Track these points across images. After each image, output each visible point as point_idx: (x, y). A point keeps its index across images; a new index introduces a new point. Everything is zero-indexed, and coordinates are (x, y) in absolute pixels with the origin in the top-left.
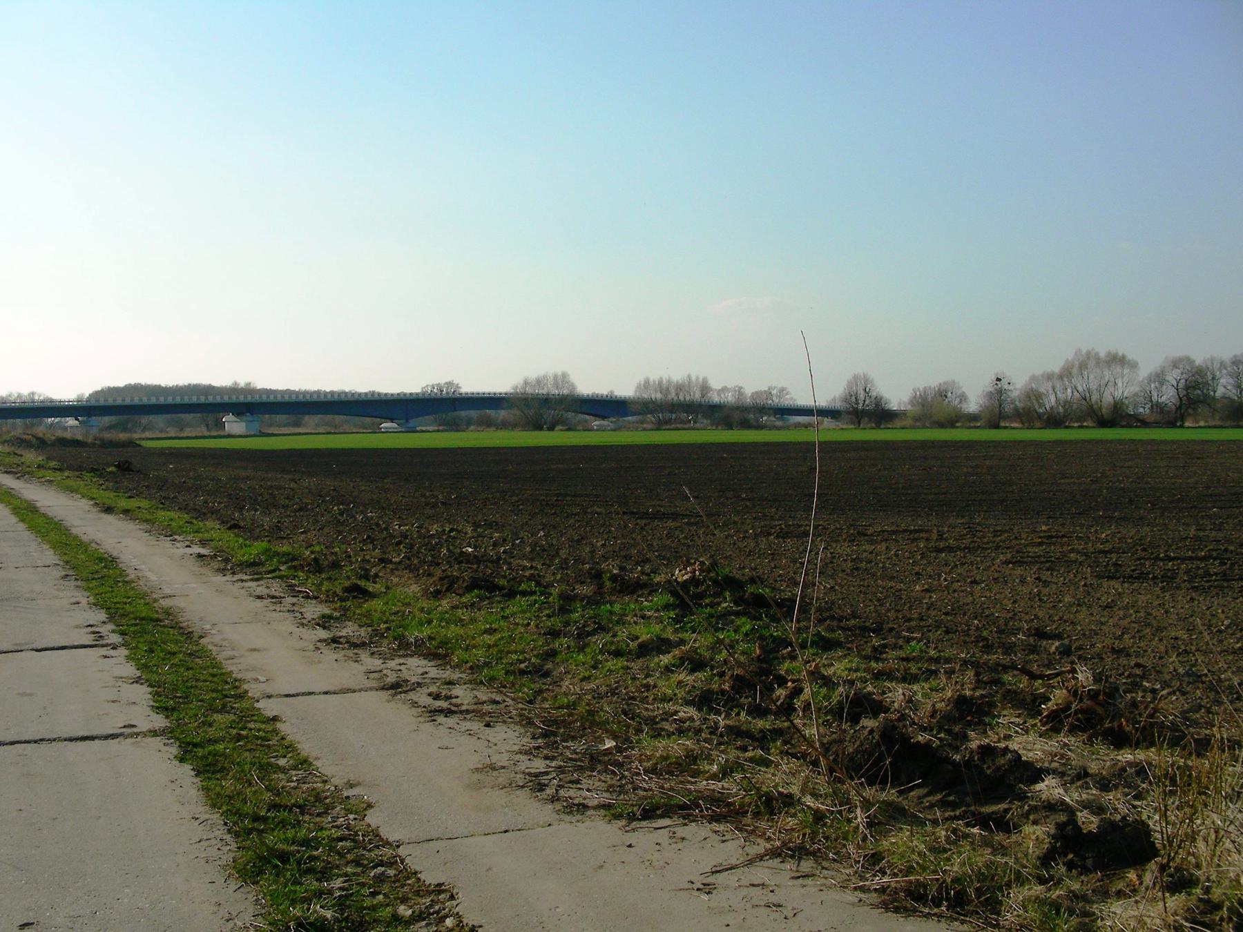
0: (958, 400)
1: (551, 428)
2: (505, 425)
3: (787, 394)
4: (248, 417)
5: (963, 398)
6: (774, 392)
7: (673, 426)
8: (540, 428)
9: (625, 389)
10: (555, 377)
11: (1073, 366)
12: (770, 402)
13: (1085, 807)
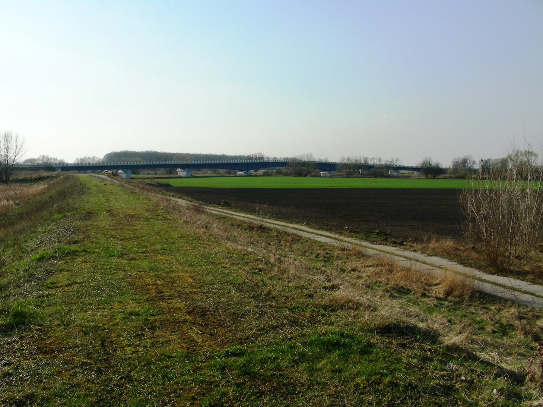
0: (472, 163)
1: (305, 176)
2: (286, 174)
3: (399, 161)
4: (187, 169)
5: (474, 163)
6: (394, 160)
7: (353, 176)
8: (300, 175)
9: (334, 158)
10: (308, 155)
11: (512, 156)
12: (392, 164)
13: (496, 379)
